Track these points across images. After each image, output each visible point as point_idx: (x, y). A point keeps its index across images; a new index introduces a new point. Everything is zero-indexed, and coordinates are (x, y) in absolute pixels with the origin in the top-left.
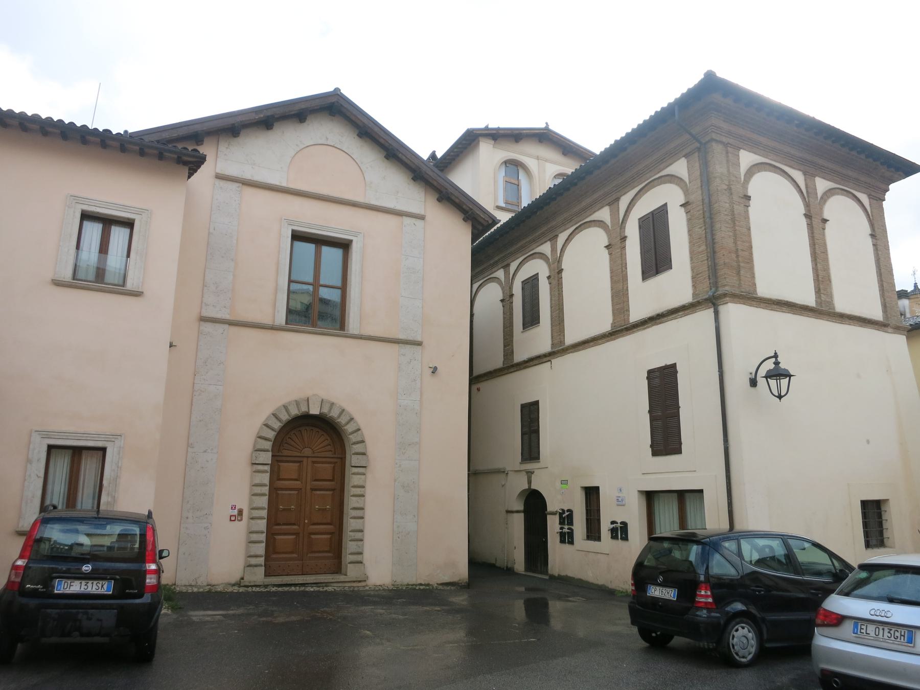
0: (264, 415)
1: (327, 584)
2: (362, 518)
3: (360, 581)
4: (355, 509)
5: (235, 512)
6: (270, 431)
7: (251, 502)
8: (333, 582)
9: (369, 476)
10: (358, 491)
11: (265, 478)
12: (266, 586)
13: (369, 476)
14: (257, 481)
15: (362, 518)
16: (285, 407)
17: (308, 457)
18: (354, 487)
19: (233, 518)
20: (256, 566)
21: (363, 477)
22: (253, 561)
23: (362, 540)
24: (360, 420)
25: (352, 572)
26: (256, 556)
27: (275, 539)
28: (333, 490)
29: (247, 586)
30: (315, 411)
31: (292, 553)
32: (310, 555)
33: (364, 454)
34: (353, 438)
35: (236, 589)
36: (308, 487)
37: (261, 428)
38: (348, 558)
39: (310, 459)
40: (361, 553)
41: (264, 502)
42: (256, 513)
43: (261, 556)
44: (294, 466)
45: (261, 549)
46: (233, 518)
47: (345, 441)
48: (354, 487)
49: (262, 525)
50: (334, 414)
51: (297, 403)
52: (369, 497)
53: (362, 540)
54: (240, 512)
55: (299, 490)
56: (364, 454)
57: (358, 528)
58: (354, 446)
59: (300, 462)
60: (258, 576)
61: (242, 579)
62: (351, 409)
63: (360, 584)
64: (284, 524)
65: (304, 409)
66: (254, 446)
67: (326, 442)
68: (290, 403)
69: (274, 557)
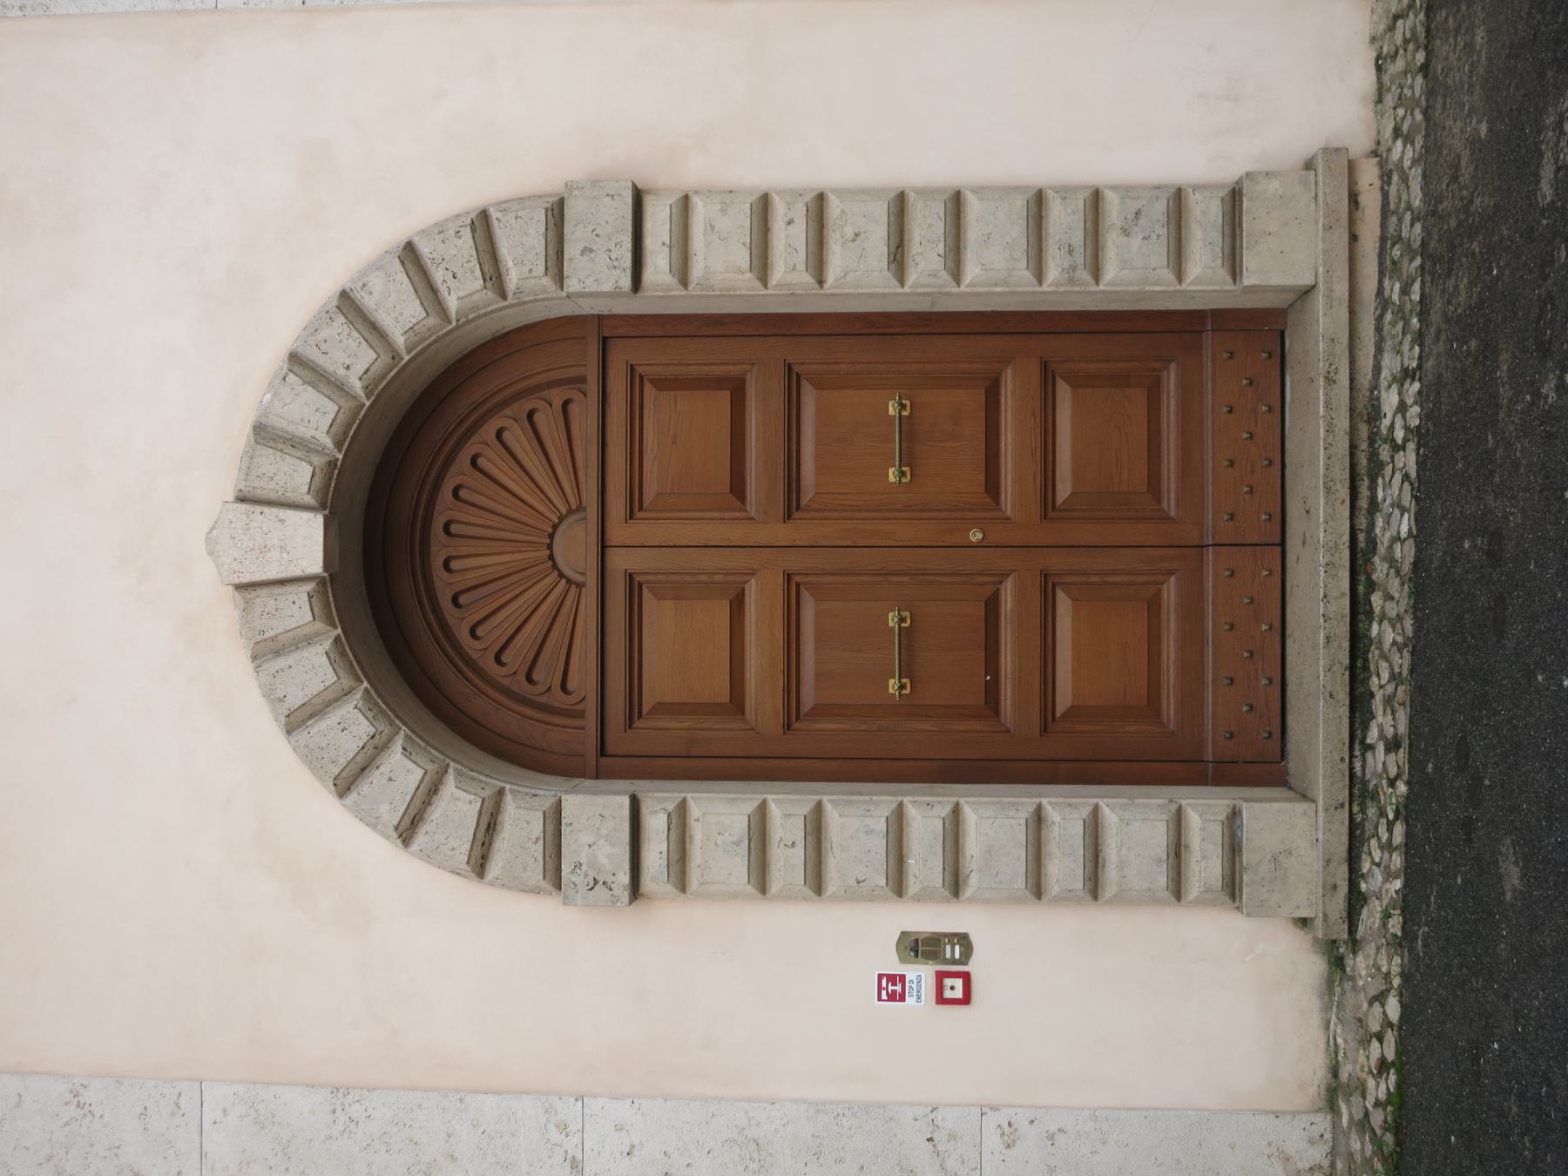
0: (350, 840)
1: (1365, 412)
2: (956, 203)
3: (1354, 199)
4: (898, 257)
5: (921, 975)
6: (436, 813)
7: (857, 893)
8: (1353, 383)
9: (696, 169)
10: (789, 241)
11: (720, 813)
12: (1359, 790)
13: (695, 170)
14: (737, 869)
15: (956, 203)
16: (296, 721)
17: (603, 547)
18: (762, 264)
19: (955, 988)
20: (1233, 848)
21: (701, 211)
22: (1205, 866)
23: (1096, 199)
24: (352, 247)
25: (1288, 255)
26: (1177, 851)
27: (1074, 712)
28: (793, 382)
29: (1356, 901)
30: (304, 543)
31: (1154, 606)
32: (1170, 504)
33: (557, 213)
34: (462, 288)
35: (1375, 963)
36: (782, 533)
37: (426, 857)
38: (1203, 278)
39: (618, 531)
40: (1178, 199)
41: (856, 819)
42: (925, 863)
43: (1178, 820)
44: (663, 623)
45: (1134, 821)
46: (955, 988)
47: (537, 314)
48: (762, 264)
49: (992, 819)
50: (315, 416)
51: (266, 651)
52: (830, 165)
53: (1096, 199)
54: (918, 947)
55: (792, 588)
56: (557, 213)
57: (1017, 232)
58: (513, 278)
59: (634, 587)
60: (1292, 831)
61: (1304, 923)
62: (292, 307)
63: (1371, 201)
64: (992, 662)
65: (296, 610)
66: (536, 891)
67: (493, 461)
68: (273, 697)
69: (1184, 733)
